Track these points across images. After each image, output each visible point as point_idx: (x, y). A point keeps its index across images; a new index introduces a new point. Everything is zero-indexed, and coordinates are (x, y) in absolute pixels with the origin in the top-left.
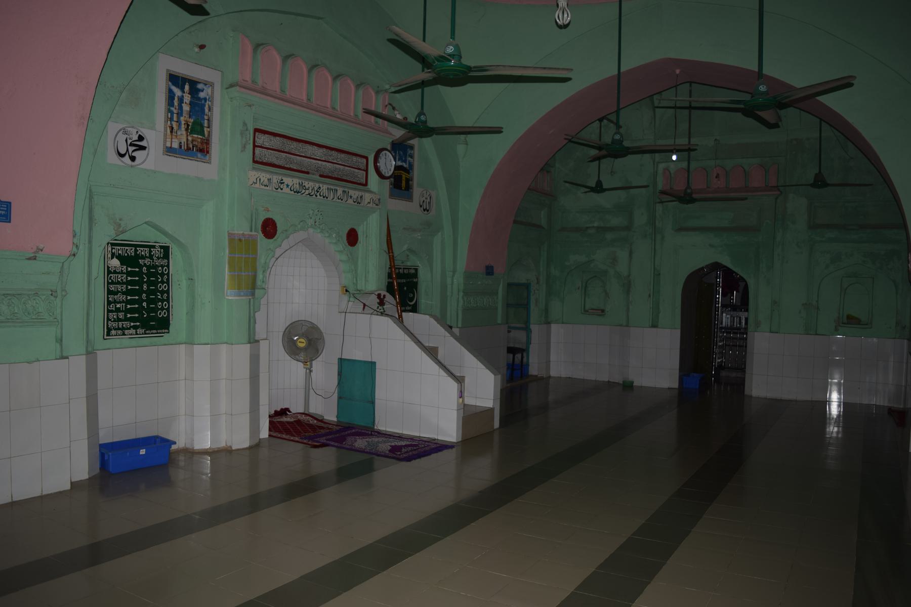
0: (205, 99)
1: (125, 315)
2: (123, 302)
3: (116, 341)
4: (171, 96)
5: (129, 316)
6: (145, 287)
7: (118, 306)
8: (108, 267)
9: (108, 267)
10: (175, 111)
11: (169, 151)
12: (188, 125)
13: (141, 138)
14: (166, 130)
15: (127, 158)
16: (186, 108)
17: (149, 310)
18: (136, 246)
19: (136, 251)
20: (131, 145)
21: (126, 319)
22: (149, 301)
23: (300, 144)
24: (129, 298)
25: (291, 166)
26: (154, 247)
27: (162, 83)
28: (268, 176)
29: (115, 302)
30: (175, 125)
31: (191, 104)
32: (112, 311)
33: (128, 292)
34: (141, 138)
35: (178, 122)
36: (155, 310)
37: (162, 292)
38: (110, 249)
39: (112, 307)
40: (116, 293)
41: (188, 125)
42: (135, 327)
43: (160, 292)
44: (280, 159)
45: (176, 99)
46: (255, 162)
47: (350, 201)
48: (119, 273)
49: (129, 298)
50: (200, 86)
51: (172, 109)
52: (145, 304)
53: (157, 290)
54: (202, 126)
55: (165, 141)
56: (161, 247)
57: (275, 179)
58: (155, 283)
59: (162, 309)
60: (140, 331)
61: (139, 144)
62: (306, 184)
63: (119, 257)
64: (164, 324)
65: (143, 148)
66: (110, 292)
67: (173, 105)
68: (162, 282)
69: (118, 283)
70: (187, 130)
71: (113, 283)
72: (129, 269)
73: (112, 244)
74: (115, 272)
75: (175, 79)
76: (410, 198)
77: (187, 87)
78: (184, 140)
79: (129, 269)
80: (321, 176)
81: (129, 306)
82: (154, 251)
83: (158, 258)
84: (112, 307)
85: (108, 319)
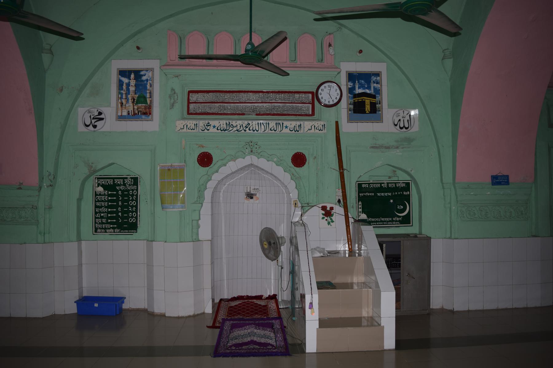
0: (147, 80)
1: (107, 221)
2: (106, 212)
3: (101, 236)
4: (120, 83)
5: (109, 221)
6: (120, 203)
7: (102, 215)
8: (96, 192)
9: (96, 192)
10: (124, 92)
11: (121, 118)
12: (134, 99)
13: (100, 113)
14: (117, 105)
15: (91, 127)
16: (132, 89)
17: (123, 218)
18: (114, 179)
19: (114, 181)
20: (93, 118)
21: (108, 223)
22: (123, 212)
23: (234, 94)
24: (109, 210)
25: (225, 112)
26: (126, 178)
27: (114, 77)
28: (195, 122)
29: (100, 212)
30: (124, 101)
31: (136, 86)
32: (98, 218)
33: (108, 207)
34: (100, 113)
35: (127, 99)
36: (128, 218)
37: (132, 207)
38: (96, 181)
39: (98, 215)
40: (101, 207)
41: (134, 99)
42: (113, 228)
43: (130, 206)
44: (215, 107)
45: (124, 85)
46: (189, 113)
47: (285, 131)
48: (103, 195)
49: (109, 210)
50: (142, 73)
51: (122, 91)
52: (120, 214)
53: (129, 205)
54: (145, 98)
55: (117, 112)
56: (131, 178)
57: (201, 123)
58: (127, 201)
59: (132, 217)
60: (116, 230)
61: (99, 117)
62: (234, 123)
63: (103, 186)
64: (133, 227)
65: (102, 119)
66: (96, 207)
67: (122, 89)
68: (133, 200)
69: (102, 201)
70: (133, 102)
71: (98, 201)
72: (110, 193)
73: (98, 178)
74: (100, 195)
75: (123, 73)
76: (380, 120)
77: (132, 76)
78: (131, 109)
79: (110, 193)
80: (257, 115)
81: (109, 215)
82: (126, 181)
83: (130, 185)
84: (98, 215)
85: (96, 223)
